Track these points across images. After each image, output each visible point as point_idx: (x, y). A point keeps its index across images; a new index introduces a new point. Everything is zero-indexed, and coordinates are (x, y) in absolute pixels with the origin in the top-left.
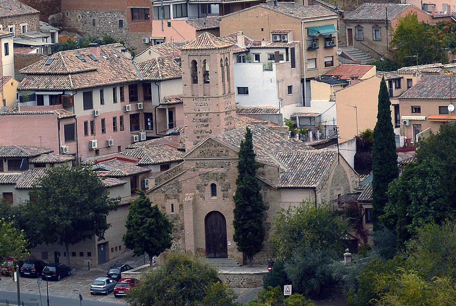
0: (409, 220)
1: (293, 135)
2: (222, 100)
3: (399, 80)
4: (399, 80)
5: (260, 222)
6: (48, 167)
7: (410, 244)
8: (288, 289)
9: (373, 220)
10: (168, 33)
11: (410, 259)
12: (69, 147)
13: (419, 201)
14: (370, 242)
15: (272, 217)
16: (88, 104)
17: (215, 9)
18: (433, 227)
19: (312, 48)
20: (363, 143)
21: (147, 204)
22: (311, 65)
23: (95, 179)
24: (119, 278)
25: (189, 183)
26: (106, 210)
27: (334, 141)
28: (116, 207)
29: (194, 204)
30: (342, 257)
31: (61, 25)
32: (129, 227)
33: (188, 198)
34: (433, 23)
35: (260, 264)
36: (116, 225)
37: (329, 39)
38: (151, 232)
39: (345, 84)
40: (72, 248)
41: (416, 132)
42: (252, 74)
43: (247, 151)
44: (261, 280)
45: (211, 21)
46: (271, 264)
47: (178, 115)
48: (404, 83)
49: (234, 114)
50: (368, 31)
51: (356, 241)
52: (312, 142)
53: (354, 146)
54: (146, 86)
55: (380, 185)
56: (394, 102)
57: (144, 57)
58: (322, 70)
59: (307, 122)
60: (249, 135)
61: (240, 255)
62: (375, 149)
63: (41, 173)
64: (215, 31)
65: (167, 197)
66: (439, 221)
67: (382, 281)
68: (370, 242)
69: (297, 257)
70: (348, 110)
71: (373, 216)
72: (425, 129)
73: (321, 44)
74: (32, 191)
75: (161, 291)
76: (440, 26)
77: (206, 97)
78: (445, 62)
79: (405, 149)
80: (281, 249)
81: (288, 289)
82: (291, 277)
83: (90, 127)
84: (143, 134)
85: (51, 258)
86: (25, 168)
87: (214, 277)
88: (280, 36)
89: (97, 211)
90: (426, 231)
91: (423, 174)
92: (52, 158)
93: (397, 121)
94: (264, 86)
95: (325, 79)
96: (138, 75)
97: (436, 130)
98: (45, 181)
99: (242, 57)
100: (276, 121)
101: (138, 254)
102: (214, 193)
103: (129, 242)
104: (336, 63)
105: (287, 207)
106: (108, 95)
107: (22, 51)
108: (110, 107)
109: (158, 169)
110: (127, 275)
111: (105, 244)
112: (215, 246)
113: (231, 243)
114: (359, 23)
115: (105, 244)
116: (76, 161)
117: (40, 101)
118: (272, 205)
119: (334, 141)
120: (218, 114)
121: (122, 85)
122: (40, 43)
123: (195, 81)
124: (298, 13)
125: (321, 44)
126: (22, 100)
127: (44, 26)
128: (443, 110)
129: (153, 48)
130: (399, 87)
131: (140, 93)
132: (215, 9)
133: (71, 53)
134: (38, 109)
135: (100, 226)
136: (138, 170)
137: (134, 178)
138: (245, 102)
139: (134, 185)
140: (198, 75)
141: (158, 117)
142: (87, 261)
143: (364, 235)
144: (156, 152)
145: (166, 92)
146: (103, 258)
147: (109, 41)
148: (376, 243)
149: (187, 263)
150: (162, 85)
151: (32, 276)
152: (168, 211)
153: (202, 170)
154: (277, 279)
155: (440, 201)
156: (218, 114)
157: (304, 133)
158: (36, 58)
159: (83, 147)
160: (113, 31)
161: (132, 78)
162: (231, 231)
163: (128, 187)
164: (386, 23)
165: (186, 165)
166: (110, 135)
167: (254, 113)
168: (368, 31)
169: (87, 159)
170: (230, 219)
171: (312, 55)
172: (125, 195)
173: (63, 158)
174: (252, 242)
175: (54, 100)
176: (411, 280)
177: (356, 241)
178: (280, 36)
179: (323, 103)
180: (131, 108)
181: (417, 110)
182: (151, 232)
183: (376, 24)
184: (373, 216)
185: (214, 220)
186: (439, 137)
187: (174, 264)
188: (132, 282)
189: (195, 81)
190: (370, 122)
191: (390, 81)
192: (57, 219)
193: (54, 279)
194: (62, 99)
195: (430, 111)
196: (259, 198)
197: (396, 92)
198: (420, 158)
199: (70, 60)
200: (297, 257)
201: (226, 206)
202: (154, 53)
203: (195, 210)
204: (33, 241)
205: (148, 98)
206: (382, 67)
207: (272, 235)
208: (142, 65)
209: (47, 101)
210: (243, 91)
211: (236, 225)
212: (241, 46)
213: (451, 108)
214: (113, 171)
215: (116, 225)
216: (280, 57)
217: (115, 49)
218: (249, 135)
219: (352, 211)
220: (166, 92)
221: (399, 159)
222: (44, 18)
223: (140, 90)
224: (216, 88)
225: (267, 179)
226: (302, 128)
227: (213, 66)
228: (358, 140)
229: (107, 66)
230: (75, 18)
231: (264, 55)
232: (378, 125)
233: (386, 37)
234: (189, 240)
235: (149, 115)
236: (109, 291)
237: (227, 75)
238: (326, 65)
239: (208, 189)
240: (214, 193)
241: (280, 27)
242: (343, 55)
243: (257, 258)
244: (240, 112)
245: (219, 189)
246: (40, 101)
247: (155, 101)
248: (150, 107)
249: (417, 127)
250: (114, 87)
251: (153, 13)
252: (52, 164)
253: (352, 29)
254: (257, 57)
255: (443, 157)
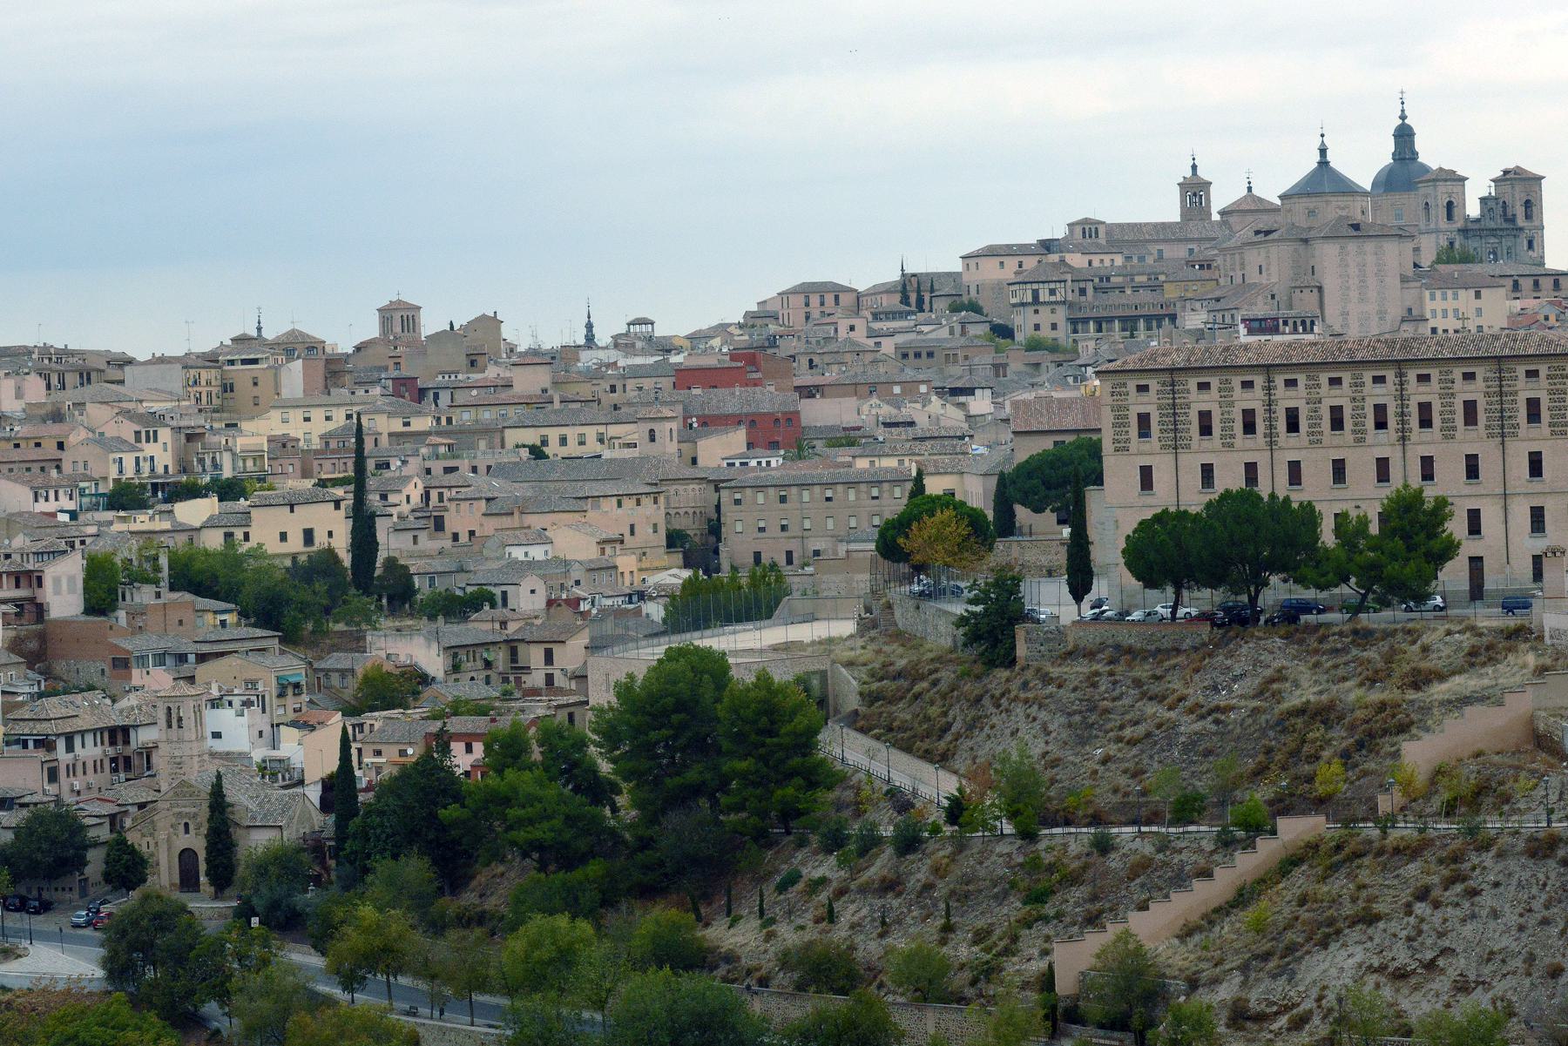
0: (368, 856)
1: (263, 777)
2: (195, 745)
3: (362, 725)
4: (362, 725)
5: (230, 859)
6: (32, 808)
7: (370, 878)
8: (255, 921)
9: (335, 856)
10: (147, 680)
11: (368, 894)
12: (52, 789)
13: (378, 838)
14: (333, 876)
15: (241, 854)
16: (70, 748)
17: (192, 658)
18: (390, 863)
19: (281, 695)
20: (328, 785)
21: (124, 842)
22: (281, 711)
23: (75, 818)
24: (98, 911)
25: (164, 820)
26: (86, 848)
27: (301, 782)
28: (96, 844)
29: (167, 842)
30: (306, 891)
31: (47, 674)
32: (107, 863)
33: (162, 836)
34: (397, 672)
35: (231, 898)
36: (95, 862)
37: (297, 686)
38: (127, 868)
39: (313, 728)
40: (54, 885)
41: (378, 773)
42: (223, 719)
43: (217, 792)
44: (230, 912)
45: (186, 669)
46: (240, 898)
47: (155, 759)
48: (366, 728)
49: (206, 757)
50: (335, 680)
51: (319, 876)
52: (281, 783)
53: (319, 787)
54: (125, 730)
55: (341, 825)
56: (354, 746)
57: (124, 703)
58: (291, 716)
59: (276, 765)
60: (219, 777)
61: (212, 889)
62: (338, 788)
63: (25, 813)
64: (191, 679)
65: (143, 836)
66: (395, 857)
67: (339, 913)
68: (333, 876)
69: (264, 890)
70: (313, 753)
71: (336, 852)
72: (386, 772)
73: (290, 691)
74: (17, 830)
75: (135, 923)
76: (403, 674)
77: (180, 740)
78: (407, 708)
79: (366, 790)
80: (249, 884)
81: (255, 921)
82: (258, 909)
83: (71, 770)
84: (122, 775)
85: (35, 893)
86: (10, 808)
87: (184, 909)
88: (252, 684)
89: (77, 849)
90: (383, 866)
91: (381, 813)
92: (35, 799)
93: (360, 763)
94: (236, 730)
95: (294, 724)
96: (117, 720)
97: (395, 771)
98: (29, 820)
99: (215, 704)
100: (246, 762)
101: (115, 889)
102: (187, 831)
103: (107, 877)
104: (304, 709)
105: (255, 843)
106: (89, 738)
107: (10, 698)
108: (90, 751)
109: (135, 809)
110: (105, 909)
111: (86, 880)
112: (188, 881)
113: (203, 879)
114: (327, 672)
115: (86, 880)
116: (58, 801)
117: (25, 745)
118: (241, 843)
119: (301, 782)
120: (191, 757)
121: (102, 730)
122: (27, 690)
123: (170, 726)
124: (268, 662)
125: (290, 691)
126: (8, 743)
127: (31, 674)
128: (403, 753)
129: (132, 696)
130: (362, 731)
131: (120, 737)
132: (192, 658)
133: (54, 700)
134: (23, 753)
135: (82, 863)
136: (117, 809)
137: (112, 817)
138: (218, 746)
139: (112, 824)
140: (173, 720)
141: (136, 761)
142: (68, 896)
143: (327, 870)
144: (133, 793)
145: (143, 737)
146: (84, 893)
147: (91, 688)
148: (339, 877)
149: (159, 897)
150: (140, 730)
151: (17, 910)
152: (144, 849)
153: (177, 810)
154: (245, 912)
155: (398, 838)
156: (191, 757)
157: (274, 775)
158: (22, 704)
159: (65, 789)
160: (96, 679)
161: (112, 723)
162: (203, 867)
163: (107, 826)
164: (352, 671)
165: (160, 805)
166: (91, 777)
167: (227, 756)
168: (335, 680)
169: (69, 799)
170: (202, 855)
171: (282, 701)
172: (104, 834)
173: (45, 799)
174: (222, 877)
175: (38, 744)
176: (367, 912)
177: (319, 876)
178: (252, 684)
179: (291, 746)
180: (111, 751)
181: (378, 753)
182: (127, 868)
183: (343, 673)
184: (336, 852)
185: (187, 856)
186: (396, 778)
187: (146, 898)
188: (110, 915)
189: (170, 726)
190: (332, 765)
191: (354, 726)
192: (39, 856)
193: (37, 912)
194: (45, 743)
195: (391, 753)
196: (228, 835)
197: (359, 737)
198: (378, 798)
199: (54, 706)
200: (264, 890)
201: (198, 844)
202: (131, 701)
203: (169, 849)
204: (16, 878)
205: (127, 742)
206: (350, 711)
207: (241, 871)
208: (121, 711)
209: (31, 744)
210: (217, 735)
211: (208, 861)
212: (215, 693)
213: (410, 751)
214: (93, 812)
215: (95, 862)
216: (252, 704)
217: (96, 697)
218: (219, 777)
219: (315, 846)
220: (143, 737)
221: (360, 798)
222: (30, 666)
223: (118, 734)
224: (189, 732)
225: (236, 818)
226: (273, 770)
227: (187, 712)
228: (323, 780)
229: (88, 711)
230: (60, 667)
231: (237, 701)
232: (340, 767)
233: (353, 684)
234: (164, 875)
235: (127, 760)
236: (89, 924)
237: (199, 721)
238: (295, 711)
239: (182, 828)
240: (187, 831)
241: (251, 675)
242: (311, 701)
243: (227, 892)
244: (213, 755)
245: (191, 827)
246: (25, 745)
247: (133, 745)
248: (129, 751)
249: (379, 769)
250: (94, 731)
251: (133, 662)
252: (36, 804)
253: (319, 680)
254: (230, 704)
255: (400, 797)
